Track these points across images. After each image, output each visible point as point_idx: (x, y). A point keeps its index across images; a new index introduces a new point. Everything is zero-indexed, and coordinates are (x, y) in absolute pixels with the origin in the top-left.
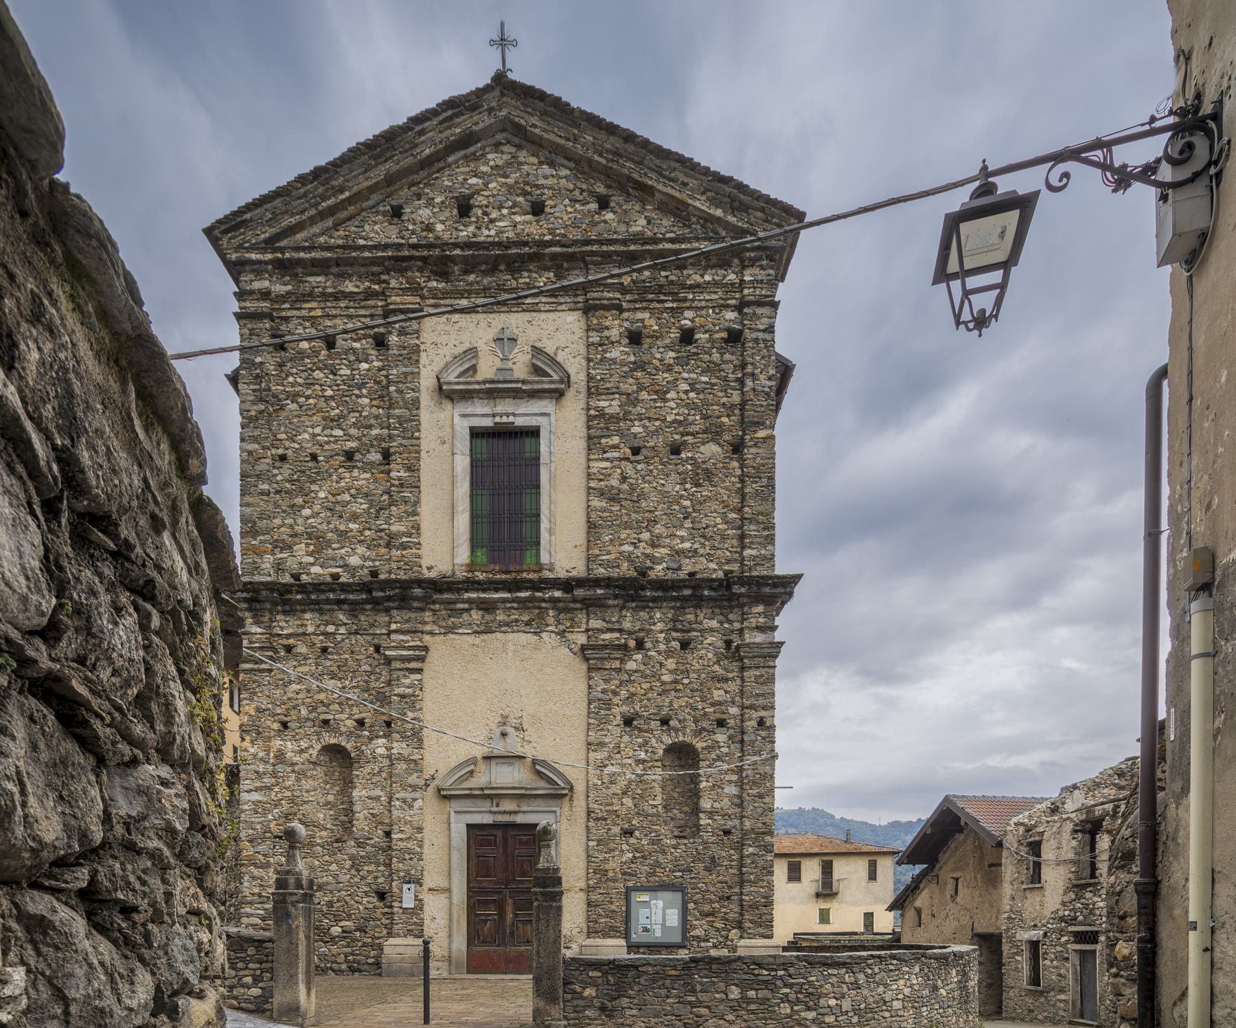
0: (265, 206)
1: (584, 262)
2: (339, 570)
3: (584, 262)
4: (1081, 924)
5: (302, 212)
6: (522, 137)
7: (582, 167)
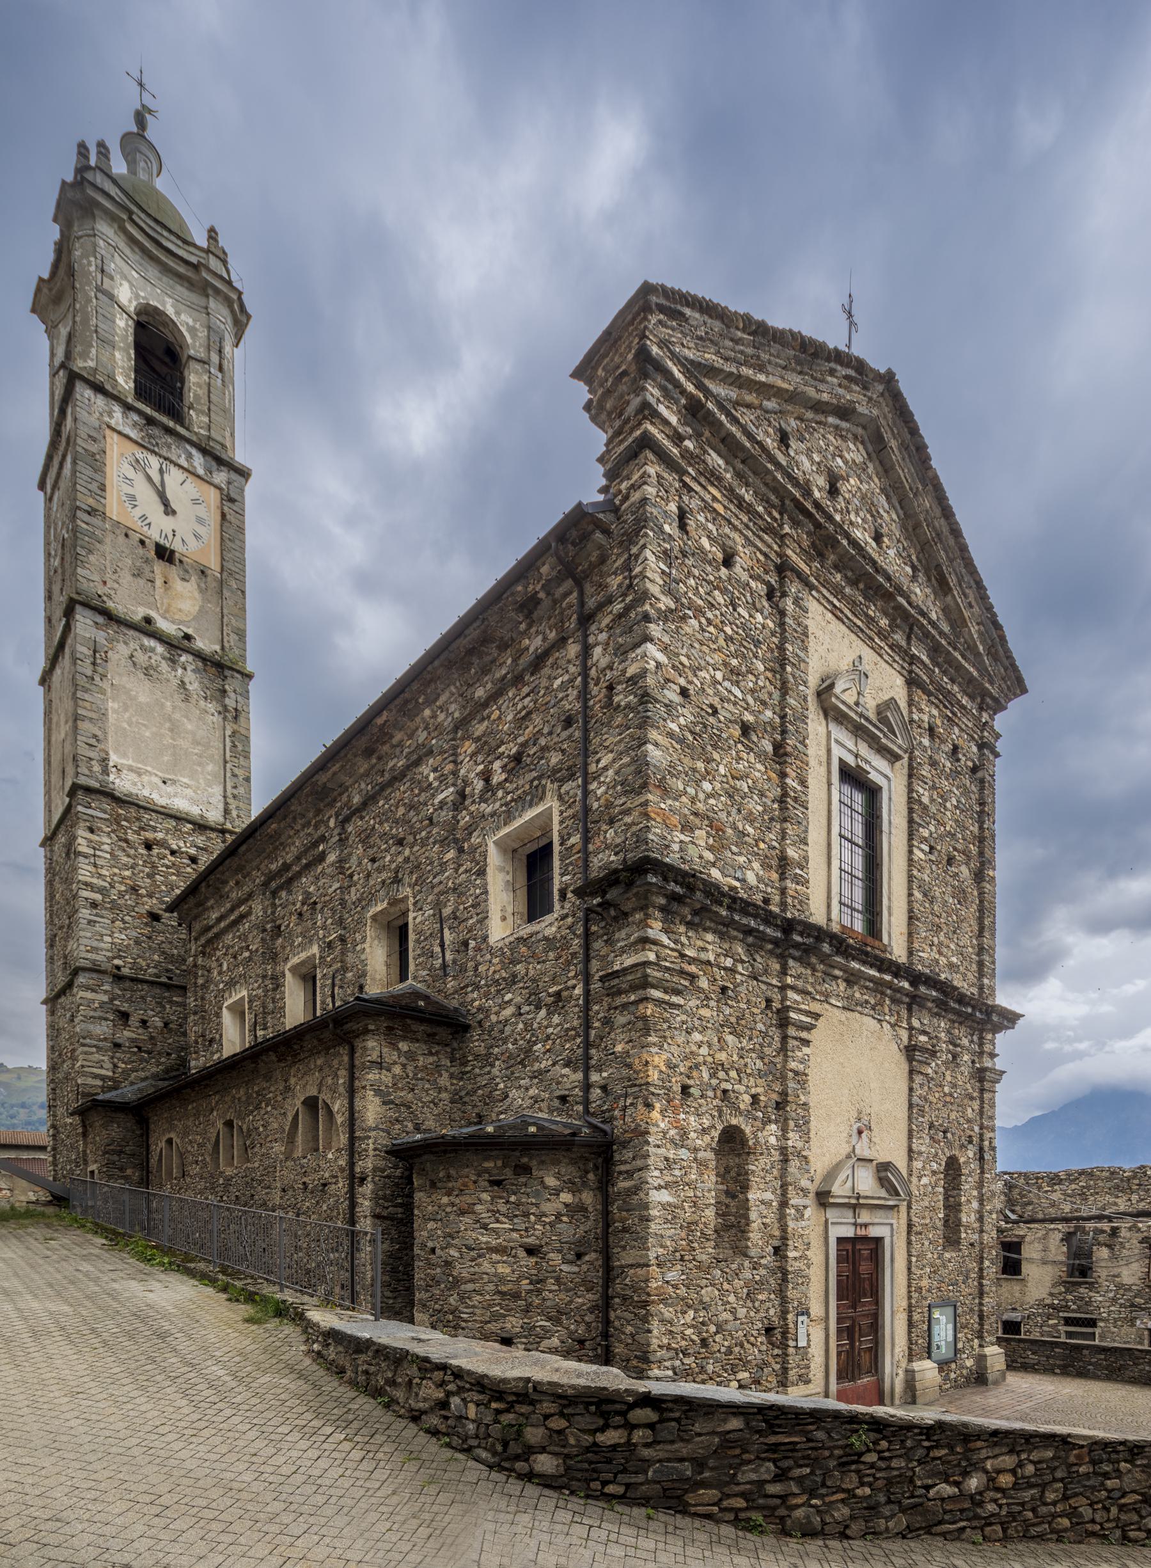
1: (911, 629)
2: (737, 884)
3: (911, 629)
4: (1074, 1311)
6: (876, 447)
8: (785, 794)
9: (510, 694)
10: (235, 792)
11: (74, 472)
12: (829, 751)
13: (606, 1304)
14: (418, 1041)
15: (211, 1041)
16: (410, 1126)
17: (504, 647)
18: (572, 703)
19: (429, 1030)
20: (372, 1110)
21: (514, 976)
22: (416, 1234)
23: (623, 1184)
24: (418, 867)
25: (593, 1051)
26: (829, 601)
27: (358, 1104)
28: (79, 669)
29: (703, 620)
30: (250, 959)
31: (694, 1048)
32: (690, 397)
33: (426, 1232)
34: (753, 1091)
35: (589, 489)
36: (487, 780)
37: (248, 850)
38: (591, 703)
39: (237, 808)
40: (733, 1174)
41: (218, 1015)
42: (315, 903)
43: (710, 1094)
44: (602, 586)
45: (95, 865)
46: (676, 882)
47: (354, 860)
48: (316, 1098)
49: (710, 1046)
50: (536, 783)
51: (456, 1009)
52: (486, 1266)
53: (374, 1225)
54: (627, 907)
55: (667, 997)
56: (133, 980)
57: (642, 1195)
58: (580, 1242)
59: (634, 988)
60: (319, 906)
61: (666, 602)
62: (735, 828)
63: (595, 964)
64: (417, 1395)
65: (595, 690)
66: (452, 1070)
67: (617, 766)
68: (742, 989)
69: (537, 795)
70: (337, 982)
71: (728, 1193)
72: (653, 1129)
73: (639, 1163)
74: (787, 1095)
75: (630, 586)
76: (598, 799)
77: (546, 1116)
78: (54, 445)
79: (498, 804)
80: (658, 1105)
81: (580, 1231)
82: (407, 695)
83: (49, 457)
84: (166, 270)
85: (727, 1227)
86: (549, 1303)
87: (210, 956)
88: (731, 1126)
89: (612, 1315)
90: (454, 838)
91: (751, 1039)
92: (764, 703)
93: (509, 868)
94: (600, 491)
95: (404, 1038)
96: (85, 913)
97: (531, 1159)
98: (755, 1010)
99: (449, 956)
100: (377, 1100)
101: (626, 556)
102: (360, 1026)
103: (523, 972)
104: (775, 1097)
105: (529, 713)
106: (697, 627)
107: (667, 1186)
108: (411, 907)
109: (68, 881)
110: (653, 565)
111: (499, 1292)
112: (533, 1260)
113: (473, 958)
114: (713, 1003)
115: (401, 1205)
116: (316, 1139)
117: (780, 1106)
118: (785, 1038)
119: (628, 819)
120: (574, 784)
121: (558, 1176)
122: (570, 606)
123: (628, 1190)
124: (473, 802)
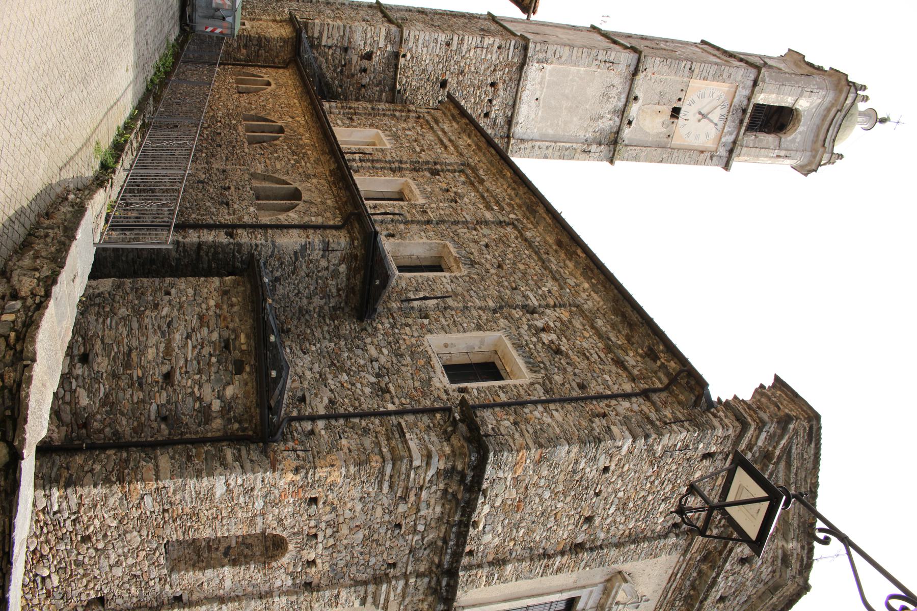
0: (812, 458)
2: (481, 528)
5: (796, 474)
7: (735, 415)
8: (549, 557)
9: (599, 344)
10: (536, 147)
11: (711, 63)
12: (584, 587)
13: (120, 444)
14: (348, 279)
15: (351, 119)
16: (278, 274)
17: (629, 338)
18: (595, 388)
19: (357, 288)
20: (290, 241)
21: (402, 356)
22: (183, 279)
23: (229, 454)
24: (483, 279)
25: (342, 421)
26: (679, 569)
27: (295, 232)
28: (601, 52)
29: (653, 478)
30: (414, 151)
31: (349, 505)
32: (773, 453)
33: (184, 287)
34: (318, 561)
35: (719, 391)
36: (543, 330)
37: (491, 154)
38: (595, 402)
39: (525, 149)
40: (246, 551)
41: (372, 125)
42: (456, 202)
43: (312, 523)
44: (665, 403)
45: (476, 47)
46: (473, 477)
47: (486, 231)
48: (300, 198)
49: (352, 519)
50: (542, 365)
51: (375, 310)
52: (153, 339)
53: (192, 244)
54: (454, 441)
55: (387, 478)
56: (396, 66)
57: (220, 470)
58: (178, 420)
59: (392, 450)
60: (453, 204)
61: (659, 449)
62: (521, 521)
63: (411, 418)
64: (24, 275)
65: (602, 404)
66: (326, 308)
67: (554, 424)
68: (401, 542)
69: (533, 367)
70: (397, 217)
71: (229, 548)
72: (277, 474)
73: (248, 465)
74: (318, 591)
75: (666, 423)
76: (531, 412)
77: (288, 386)
78: (725, 52)
79: (527, 338)
80: (298, 478)
81: (186, 419)
82: (596, 271)
83: (718, 49)
84: (819, 128)
85: (198, 551)
86: (121, 394)
87: (417, 122)
88: (287, 544)
89: (111, 452)
90: (502, 308)
91: (362, 553)
92: (608, 531)
93: (484, 349)
94: (719, 399)
95: (349, 268)
96: (442, 38)
97: (249, 373)
98: (385, 555)
99: (416, 304)
100: (298, 247)
101: (683, 419)
102: (357, 234)
103: (404, 362)
104: (315, 581)
105: (588, 359)
106: (648, 474)
107: (229, 491)
108: (453, 274)
109: (464, 28)
110: (681, 437)
111: (130, 351)
112: (160, 380)
113: (415, 323)
114: (387, 517)
115: (210, 266)
116: (268, 198)
117: (308, 586)
118: (365, 583)
119: (517, 435)
120: (541, 394)
121: (235, 398)
122: (653, 383)
123: (225, 458)
124: (528, 320)
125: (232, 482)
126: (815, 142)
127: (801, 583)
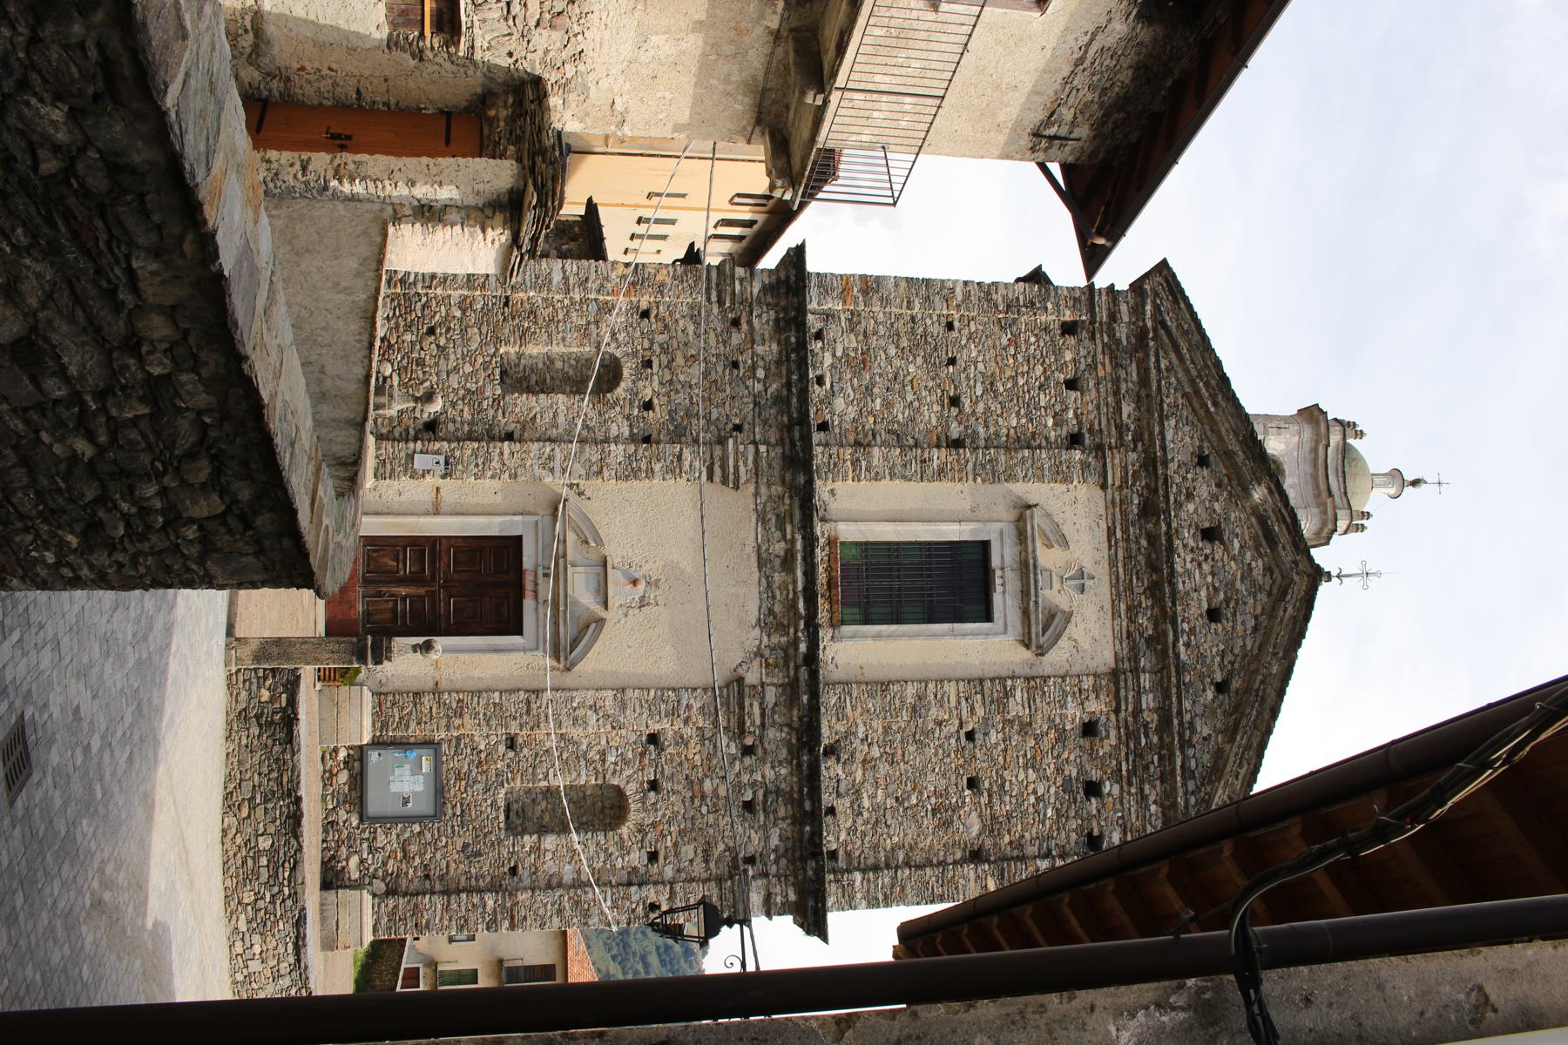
2: (828, 385)
32: (1145, 325)
34: (656, 401)
84: (1315, 477)
125: (568, 268)
126: (1318, 496)
127: (1309, 571)
